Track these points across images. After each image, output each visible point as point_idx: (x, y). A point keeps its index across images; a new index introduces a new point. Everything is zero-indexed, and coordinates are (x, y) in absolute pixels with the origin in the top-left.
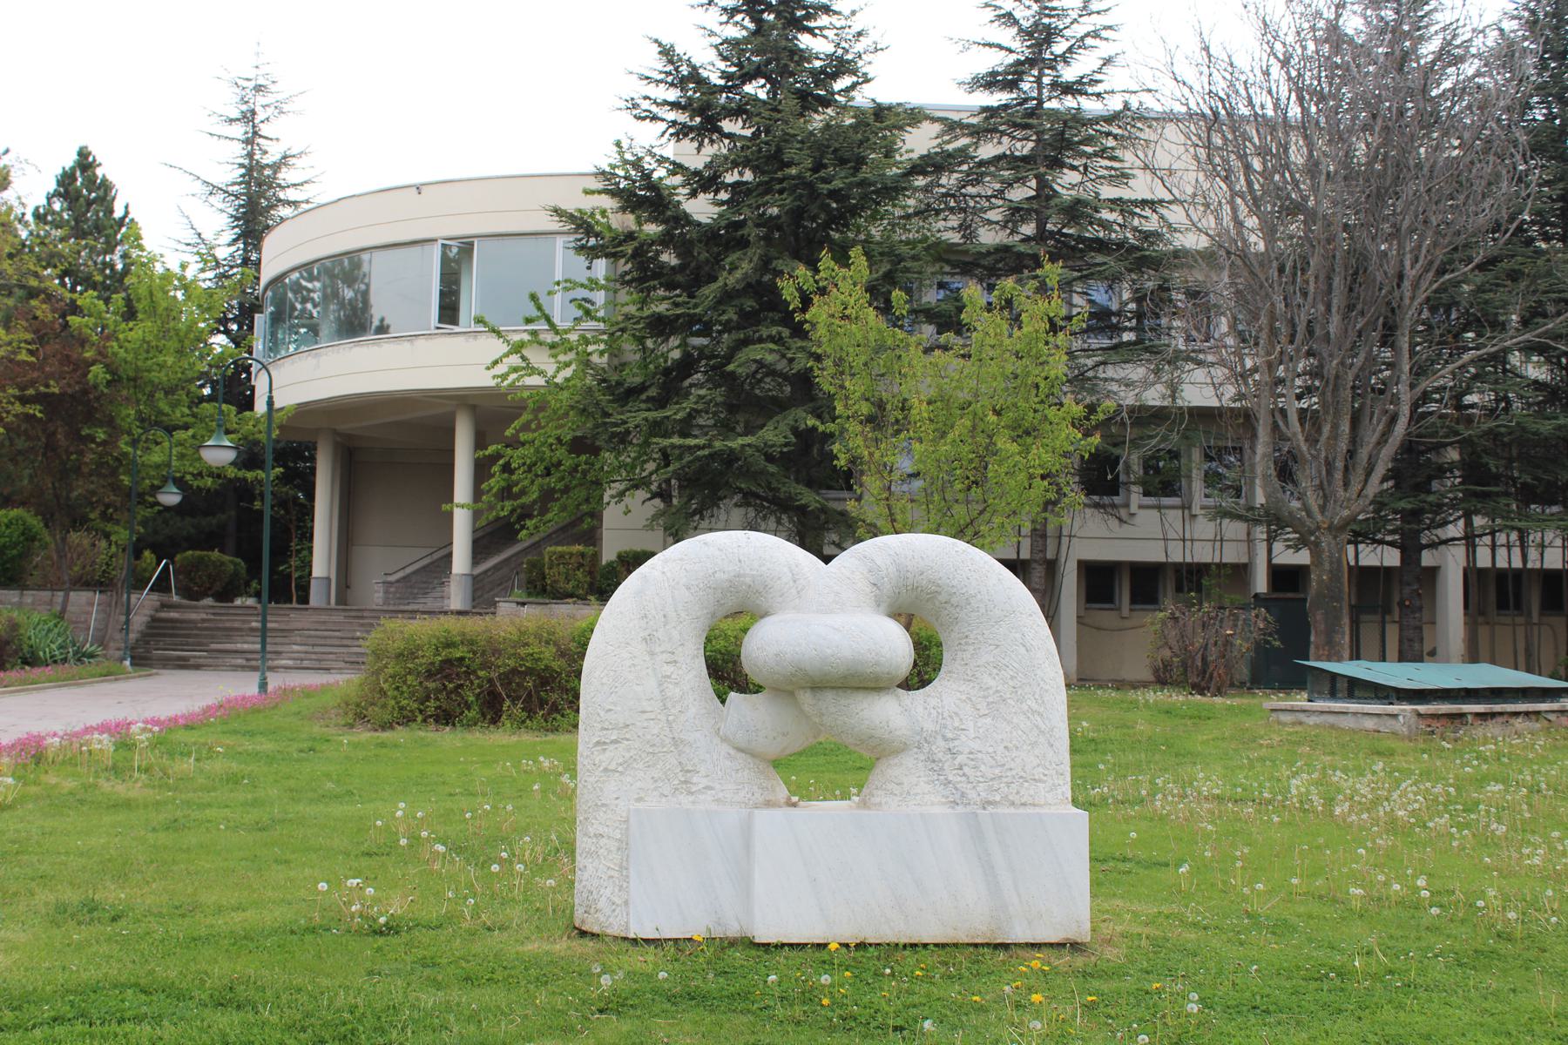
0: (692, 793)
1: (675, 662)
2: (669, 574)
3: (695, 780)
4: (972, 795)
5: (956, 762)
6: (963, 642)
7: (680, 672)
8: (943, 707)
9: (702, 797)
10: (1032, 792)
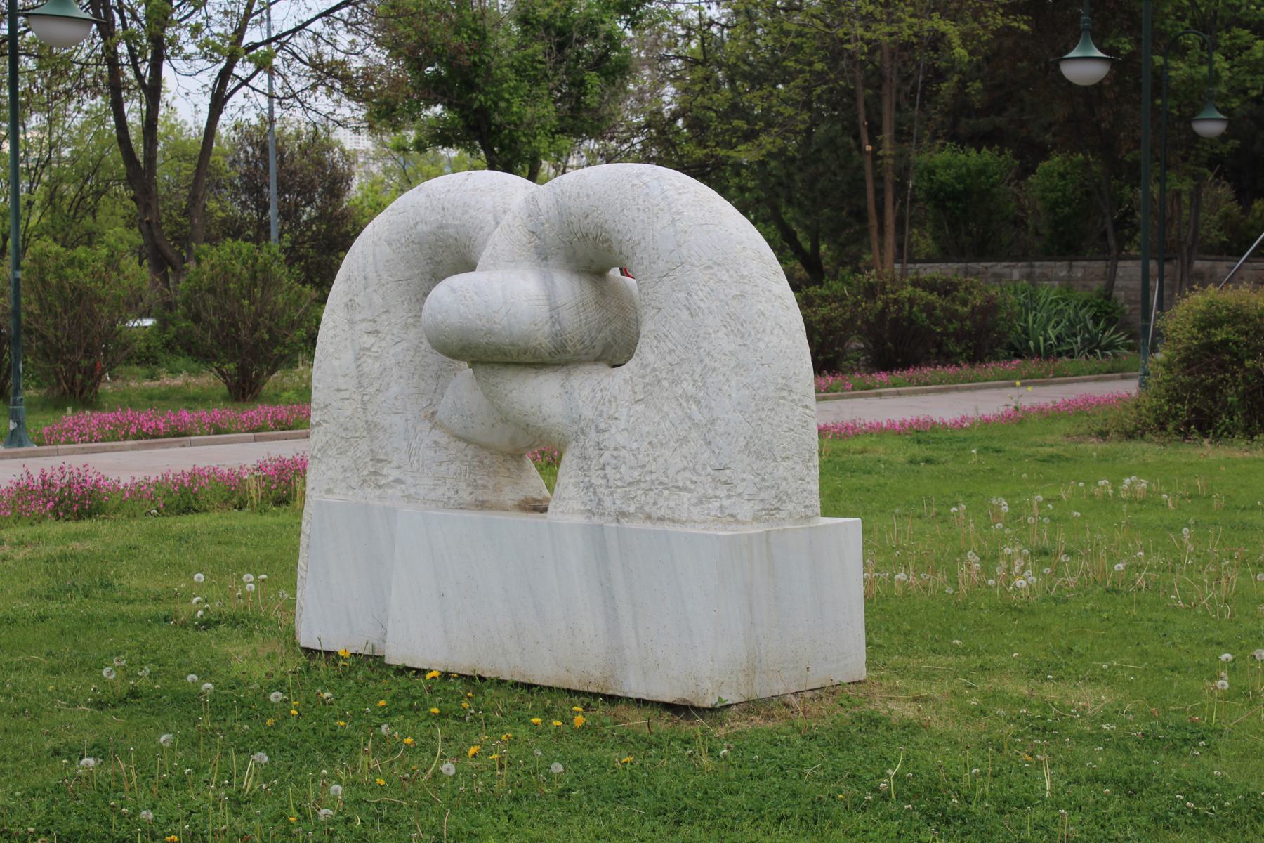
0: (380, 487)
1: (377, 332)
3: (385, 471)
7: (384, 344)
9: (390, 492)
10: (672, 504)
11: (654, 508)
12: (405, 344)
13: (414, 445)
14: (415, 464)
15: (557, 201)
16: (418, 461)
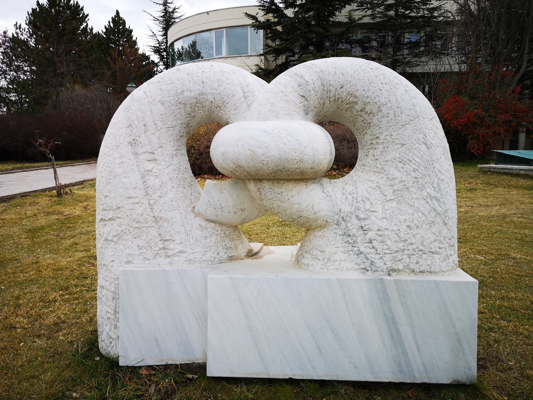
0: (169, 257)
1: (155, 160)
2: (148, 93)
3: (171, 247)
4: (379, 263)
5: (367, 237)
6: (374, 142)
7: (160, 167)
8: (357, 193)
9: (176, 259)
10: (429, 262)
11: (417, 266)
12: (172, 167)
13: (188, 229)
14: (191, 240)
15: (320, 77)
16: (192, 238)
